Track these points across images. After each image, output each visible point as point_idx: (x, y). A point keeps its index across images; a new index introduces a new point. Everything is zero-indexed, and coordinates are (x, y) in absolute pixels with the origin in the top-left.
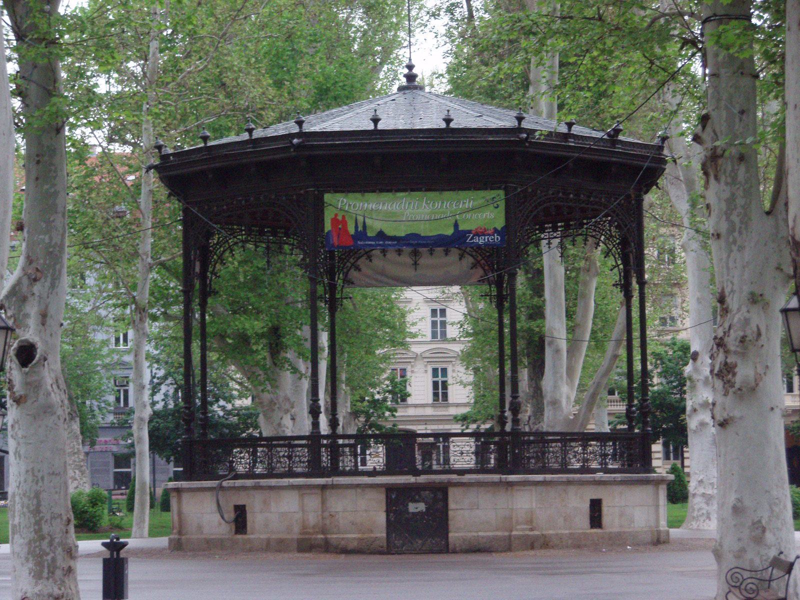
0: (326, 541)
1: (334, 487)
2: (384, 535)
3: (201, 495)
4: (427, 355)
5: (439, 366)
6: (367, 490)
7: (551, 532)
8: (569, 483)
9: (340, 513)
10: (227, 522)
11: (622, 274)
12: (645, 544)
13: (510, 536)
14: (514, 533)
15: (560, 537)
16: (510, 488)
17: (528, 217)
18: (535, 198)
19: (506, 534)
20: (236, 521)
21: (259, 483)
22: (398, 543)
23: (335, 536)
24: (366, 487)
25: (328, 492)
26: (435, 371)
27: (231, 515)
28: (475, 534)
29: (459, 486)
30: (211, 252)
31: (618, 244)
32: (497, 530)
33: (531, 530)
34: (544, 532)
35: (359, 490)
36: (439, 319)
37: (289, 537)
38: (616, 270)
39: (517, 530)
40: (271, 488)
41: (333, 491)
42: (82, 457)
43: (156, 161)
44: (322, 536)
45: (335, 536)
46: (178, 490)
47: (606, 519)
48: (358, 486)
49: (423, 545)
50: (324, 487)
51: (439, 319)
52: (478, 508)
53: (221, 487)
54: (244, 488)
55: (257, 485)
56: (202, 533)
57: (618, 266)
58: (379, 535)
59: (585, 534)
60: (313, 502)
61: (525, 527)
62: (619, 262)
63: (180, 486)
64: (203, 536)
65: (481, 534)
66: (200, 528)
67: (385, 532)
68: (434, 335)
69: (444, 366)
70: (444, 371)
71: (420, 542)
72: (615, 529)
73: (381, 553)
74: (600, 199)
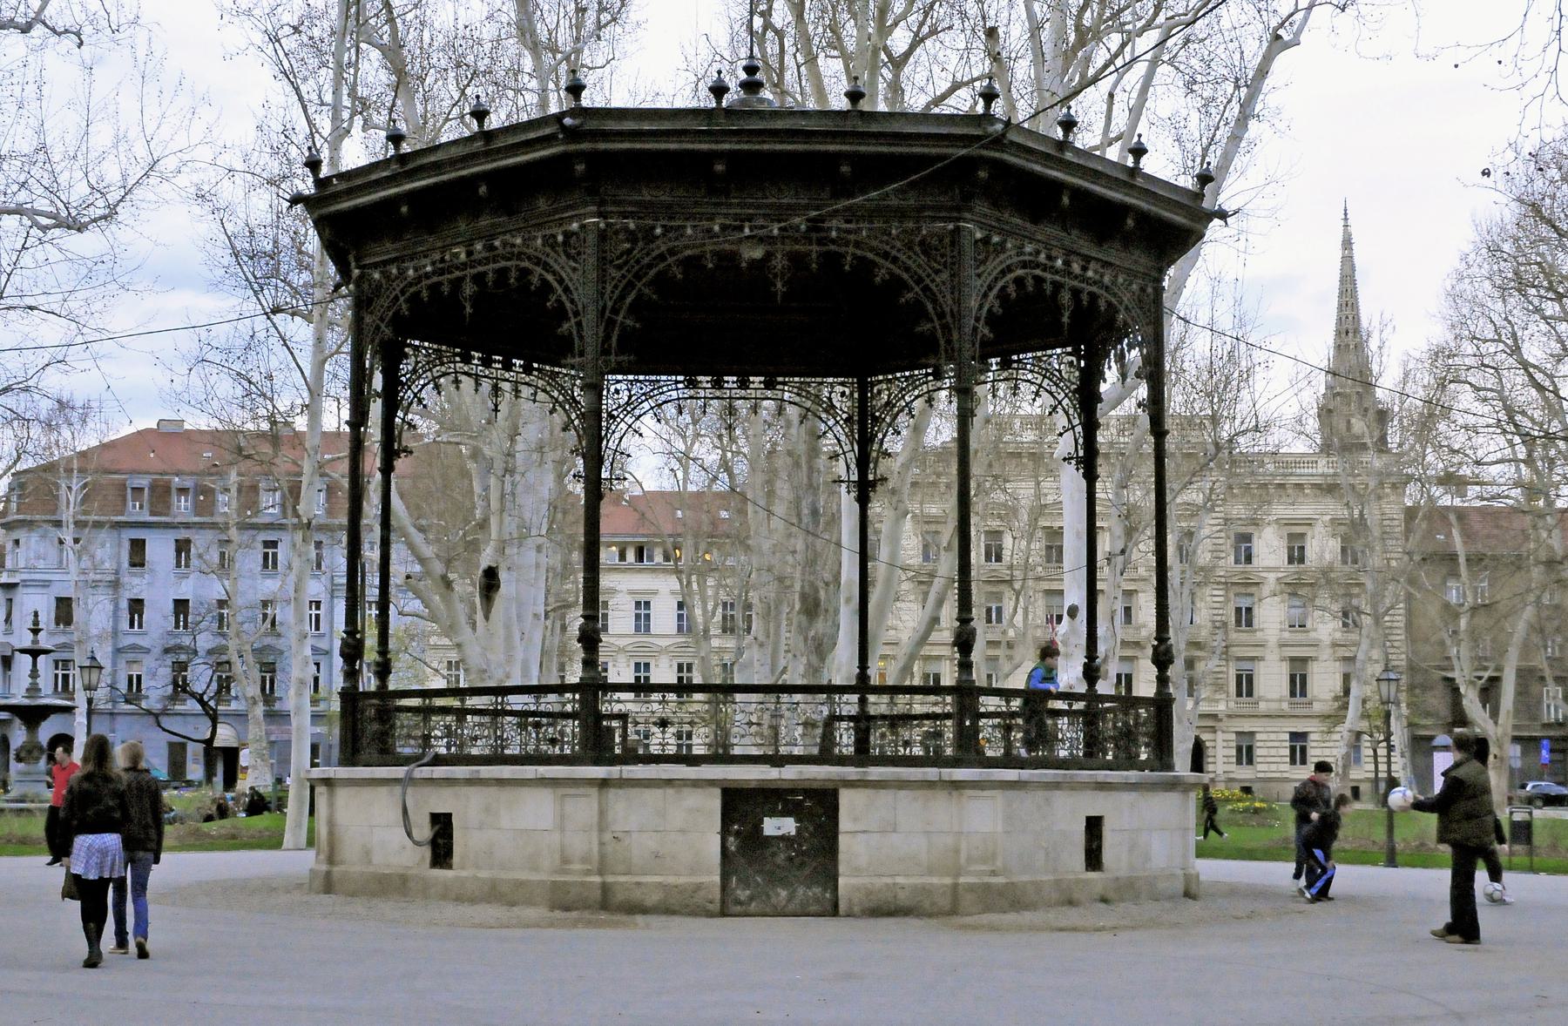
0: (605, 888)
1: (623, 783)
2: (717, 879)
3: (367, 793)
4: (629, 648)
5: (642, 661)
6: (686, 791)
7: (1025, 878)
8: (1056, 785)
9: (634, 836)
10: (417, 843)
11: (1081, 441)
12: (1171, 898)
13: (955, 886)
14: (962, 880)
15: (1038, 886)
16: (955, 793)
17: (990, 288)
18: (1002, 257)
19: (948, 881)
20: (434, 843)
21: (478, 771)
22: (743, 894)
23: (622, 879)
24: (685, 785)
25: (612, 793)
26: (637, 665)
27: (424, 831)
28: (889, 880)
29: (859, 786)
30: (403, 384)
31: (1074, 392)
32: (931, 871)
33: (993, 873)
34: (1015, 879)
35: (670, 791)
36: (643, 612)
37: (534, 877)
38: (1069, 435)
39: (969, 873)
40: (501, 782)
41: (621, 792)
42: (264, 745)
43: (307, 186)
44: (597, 879)
45: (622, 879)
46: (328, 782)
47: (1107, 856)
48: (669, 783)
49: (790, 899)
50: (604, 783)
51: (643, 612)
52: (894, 831)
53: (410, 781)
54: (450, 782)
55: (475, 776)
56: (370, 862)
57: (1073, 428)
58: (704, 879)
59: (1078, 881)
60: (584, 807)
61: (983, 868)
62: (1076, 422)
63: (332, 776)
64: (371, 869)
65: (900, 880)
66: (367, 853)
67: (719, 871)
68: (637, 628)
69: (647, 661)
70: (647, 665)
71: (784, 893)
72: (1123, 873)
73: (710, 915)
74: (1102, 276)
